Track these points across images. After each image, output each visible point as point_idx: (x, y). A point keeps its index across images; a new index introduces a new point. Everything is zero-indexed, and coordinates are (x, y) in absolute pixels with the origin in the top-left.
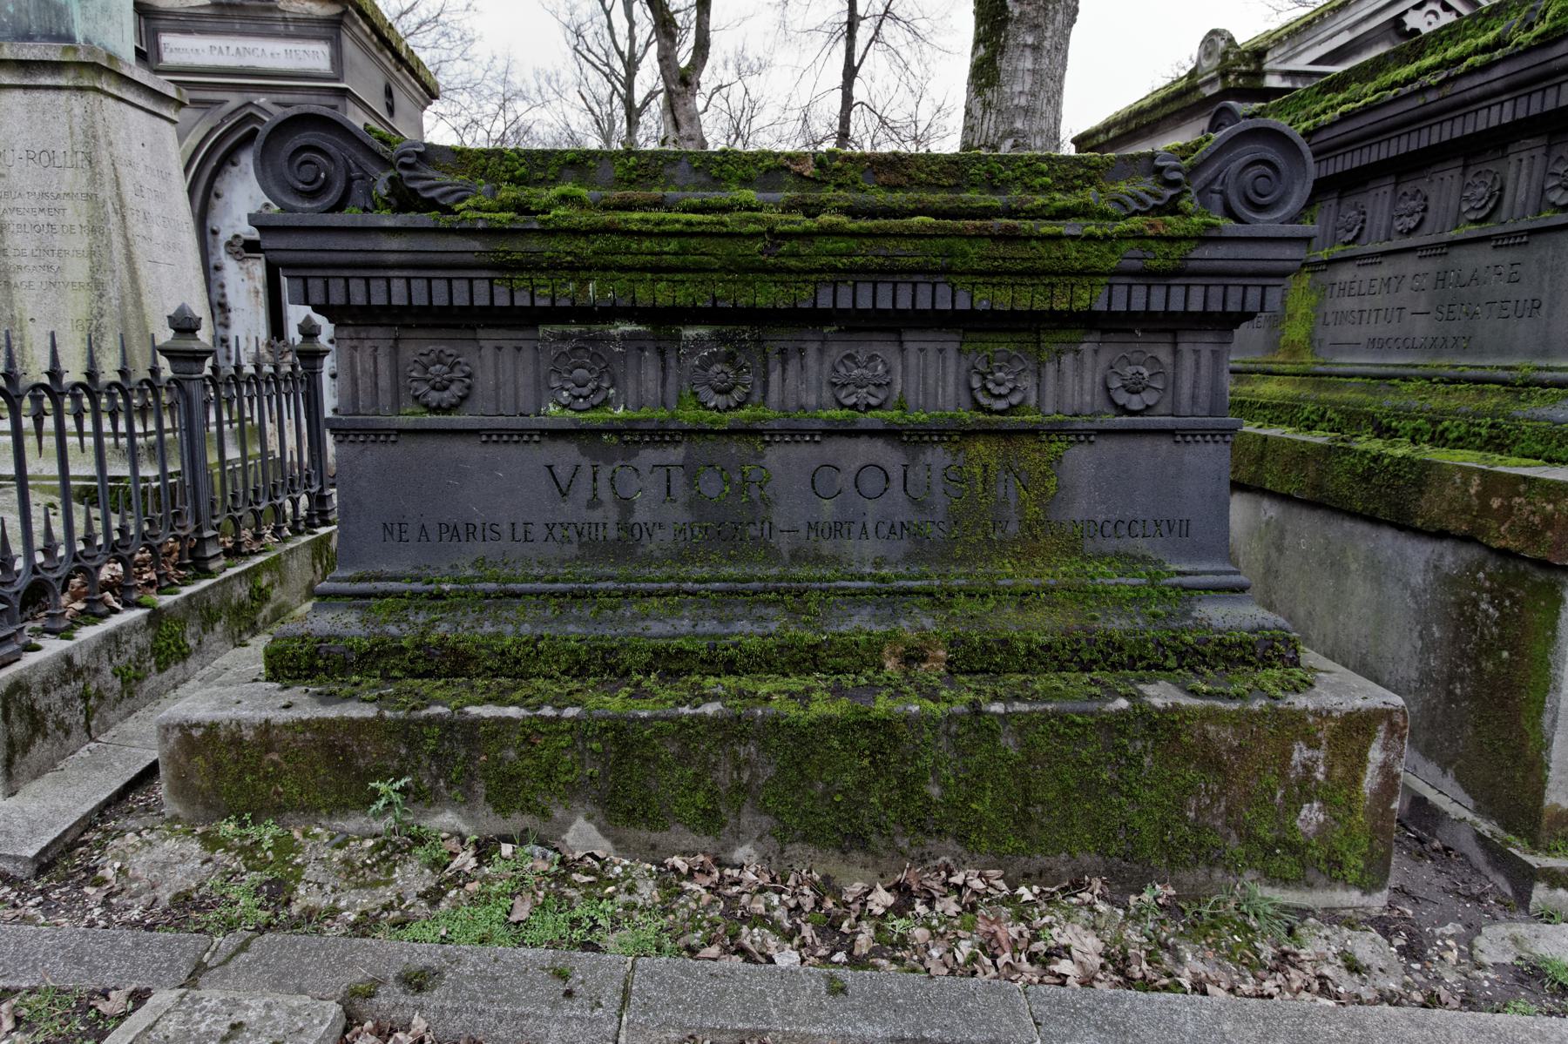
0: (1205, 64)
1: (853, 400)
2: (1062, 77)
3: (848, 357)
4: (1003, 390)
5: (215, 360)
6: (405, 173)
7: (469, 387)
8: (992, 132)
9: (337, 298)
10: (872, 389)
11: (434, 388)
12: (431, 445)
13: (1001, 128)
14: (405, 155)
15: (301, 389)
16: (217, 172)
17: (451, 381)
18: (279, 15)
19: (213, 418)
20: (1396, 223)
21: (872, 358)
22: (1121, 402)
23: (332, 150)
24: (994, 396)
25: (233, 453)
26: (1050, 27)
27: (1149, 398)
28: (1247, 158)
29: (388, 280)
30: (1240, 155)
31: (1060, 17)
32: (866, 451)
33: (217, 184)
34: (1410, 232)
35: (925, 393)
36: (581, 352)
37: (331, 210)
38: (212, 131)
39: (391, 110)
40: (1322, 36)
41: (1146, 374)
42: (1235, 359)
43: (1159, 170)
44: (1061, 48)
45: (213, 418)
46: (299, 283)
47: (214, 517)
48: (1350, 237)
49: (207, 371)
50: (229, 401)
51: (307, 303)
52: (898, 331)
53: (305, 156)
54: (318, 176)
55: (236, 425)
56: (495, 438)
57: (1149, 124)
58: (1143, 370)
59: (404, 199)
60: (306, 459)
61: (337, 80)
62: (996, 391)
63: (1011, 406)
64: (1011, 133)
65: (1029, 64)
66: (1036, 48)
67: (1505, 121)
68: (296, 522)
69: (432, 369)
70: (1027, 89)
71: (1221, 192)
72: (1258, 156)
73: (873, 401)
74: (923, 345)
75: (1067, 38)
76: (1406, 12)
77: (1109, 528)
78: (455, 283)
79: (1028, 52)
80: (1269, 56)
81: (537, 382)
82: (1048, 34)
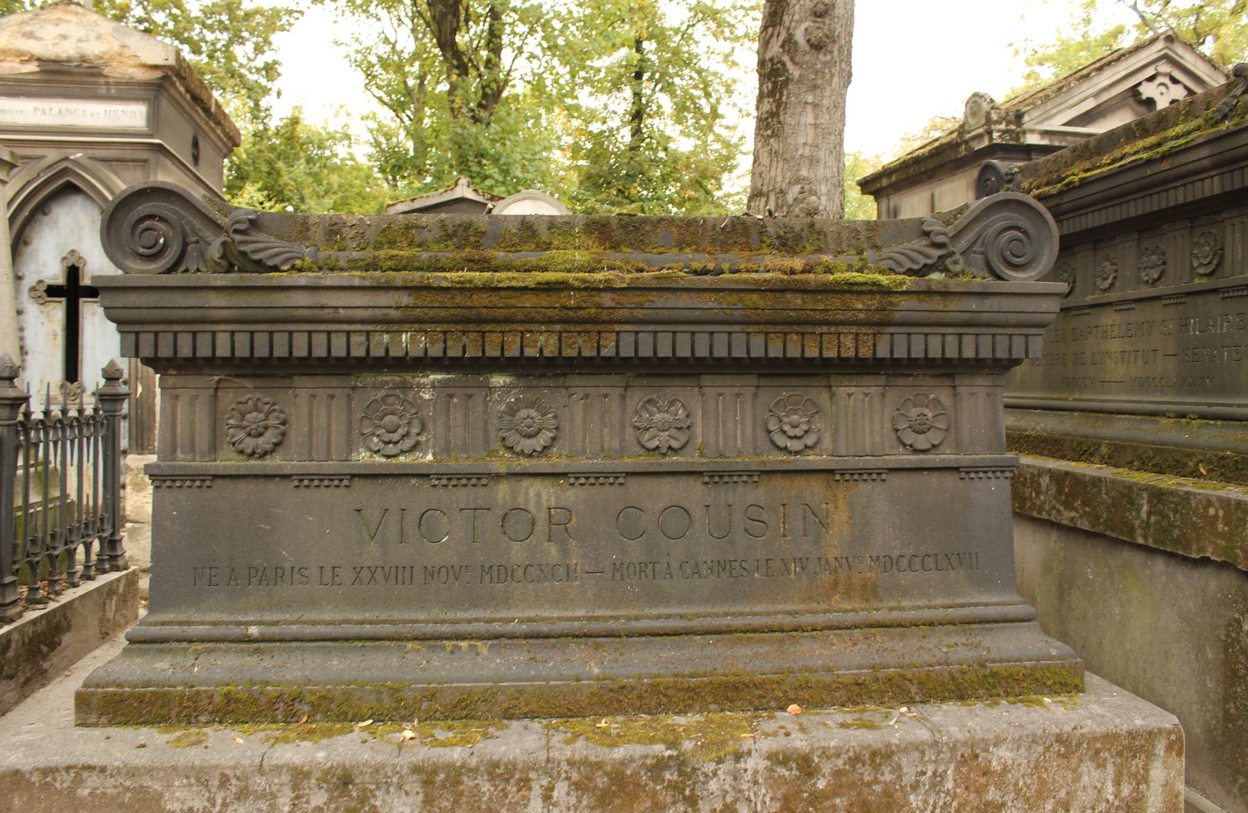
0: (972, 121)
1: (656, 443)
2: (841, 133)
3: (649, 401)
4: (798, 432)
5: (28, 406)
6: (238, 237)
7: (283, 434)
8: (779, 179)
9: (165, 351)
10: (673, 431)
11: (249, 435)
12: (242, 488)
13: (788, 175)
14: (238, 222)
15: (102, 432)
16: (29, 221)
17: (266, 428)
18: (102, 80)
19: (20, 462)
20: (1143, 274)
21: (672, 403)
22: (908, 442)
23: (165, 213)
24: (791, 438)
25: (35, 498)
26: (828, 88)
27: (934, 437)
28: (1002, 224)
29: (214, 333)
30: (995, 222)
31: (836, 79)
32: (666, 491)
33: (27, 232)
34: (1154, 282)
35: (725, 437)
36: (391, 400)
37: (169, 271)
38: (28, 183)
39: (196, 159)
40: (1071, 102)
41: (930, 415)
42: (1009, 396)
43: (927, 234)
44: (838, 107)
45: (20, 462)
46: (132, 337)
47: (15, 562)
48: (1106, 284)
49: (21, 418)
50: (36, 445)
51: (137, 356)
52: (696, 375)
53: (147, 223)
54: (157, 242)
55: (40, 468)
56: (306, 482)
57: (926, 171)
58: (926, 411)
59: (232, 260)
60: (100, 502)
61: (151, 136)
62: (792, 432)
63: (806, 447)
64: (798, 181)
65: (810, 119)
66: (815, 106)
67: (1216, 192)
68: (87, 567)
69: (248, 416)
70: (810, 141)
71: (982, 253)
72: (1010, 223)
73: (675, 445)
74: (720, 390)
75: (843, 97)
76: (1140, 84)
77: (904, 562)
78: (277, 336)
79: (809, 109)
80: (1026, 118)
81: (349, 430)
82: (827, 93)
